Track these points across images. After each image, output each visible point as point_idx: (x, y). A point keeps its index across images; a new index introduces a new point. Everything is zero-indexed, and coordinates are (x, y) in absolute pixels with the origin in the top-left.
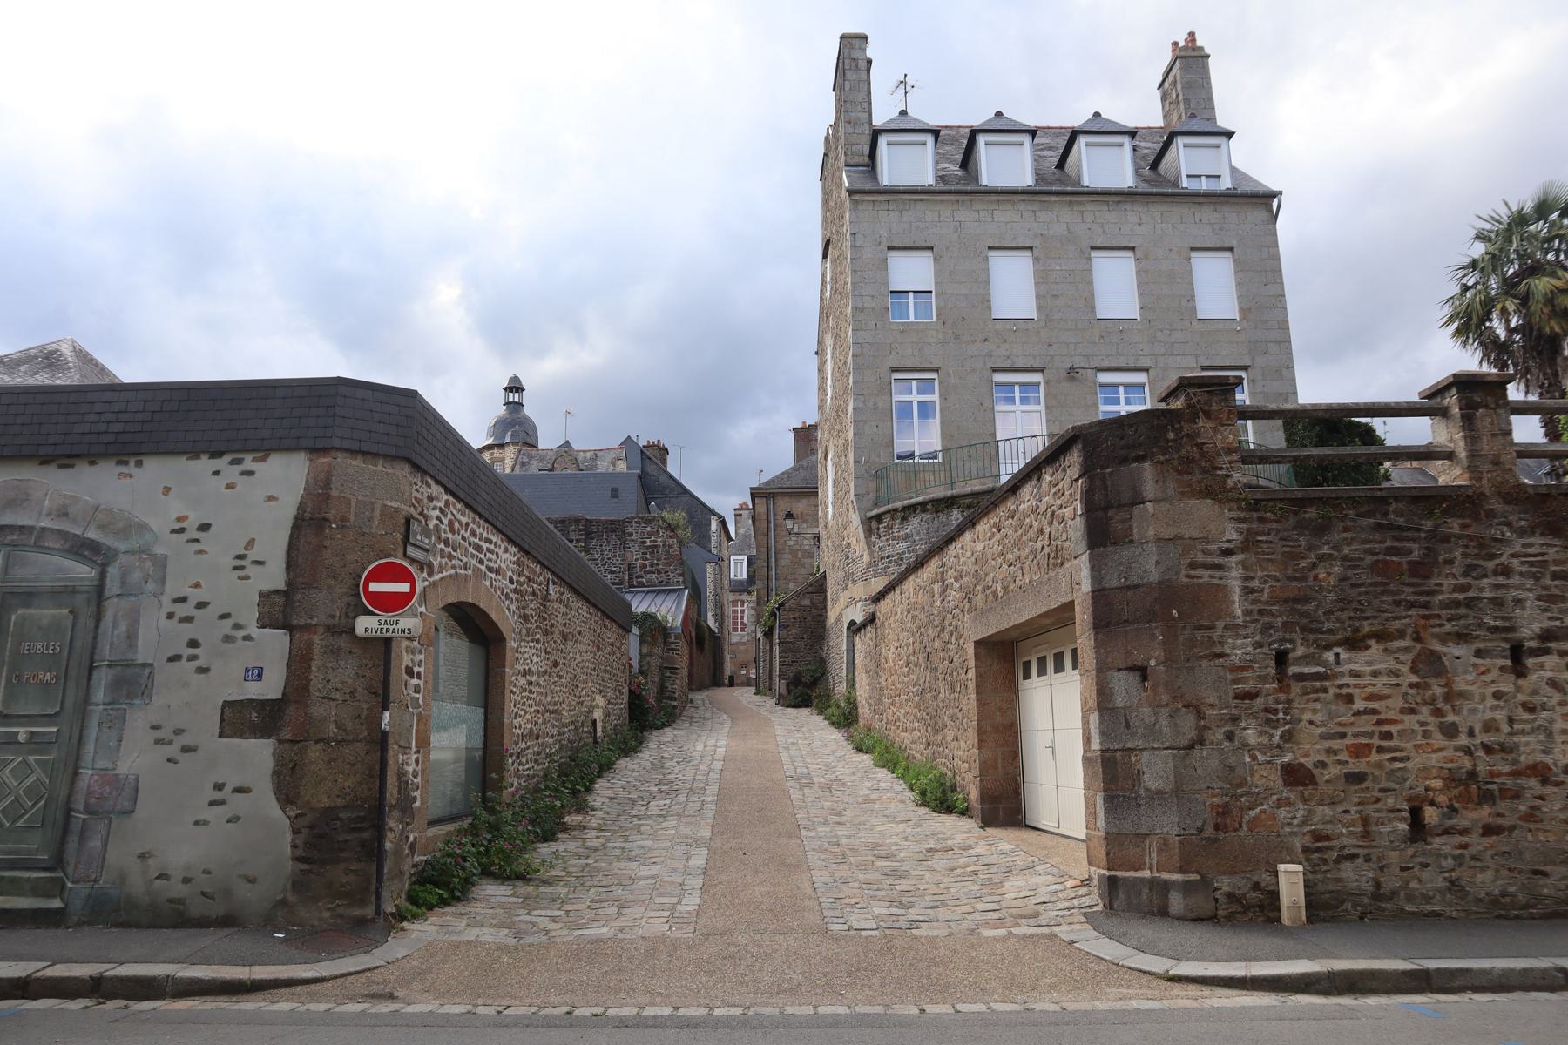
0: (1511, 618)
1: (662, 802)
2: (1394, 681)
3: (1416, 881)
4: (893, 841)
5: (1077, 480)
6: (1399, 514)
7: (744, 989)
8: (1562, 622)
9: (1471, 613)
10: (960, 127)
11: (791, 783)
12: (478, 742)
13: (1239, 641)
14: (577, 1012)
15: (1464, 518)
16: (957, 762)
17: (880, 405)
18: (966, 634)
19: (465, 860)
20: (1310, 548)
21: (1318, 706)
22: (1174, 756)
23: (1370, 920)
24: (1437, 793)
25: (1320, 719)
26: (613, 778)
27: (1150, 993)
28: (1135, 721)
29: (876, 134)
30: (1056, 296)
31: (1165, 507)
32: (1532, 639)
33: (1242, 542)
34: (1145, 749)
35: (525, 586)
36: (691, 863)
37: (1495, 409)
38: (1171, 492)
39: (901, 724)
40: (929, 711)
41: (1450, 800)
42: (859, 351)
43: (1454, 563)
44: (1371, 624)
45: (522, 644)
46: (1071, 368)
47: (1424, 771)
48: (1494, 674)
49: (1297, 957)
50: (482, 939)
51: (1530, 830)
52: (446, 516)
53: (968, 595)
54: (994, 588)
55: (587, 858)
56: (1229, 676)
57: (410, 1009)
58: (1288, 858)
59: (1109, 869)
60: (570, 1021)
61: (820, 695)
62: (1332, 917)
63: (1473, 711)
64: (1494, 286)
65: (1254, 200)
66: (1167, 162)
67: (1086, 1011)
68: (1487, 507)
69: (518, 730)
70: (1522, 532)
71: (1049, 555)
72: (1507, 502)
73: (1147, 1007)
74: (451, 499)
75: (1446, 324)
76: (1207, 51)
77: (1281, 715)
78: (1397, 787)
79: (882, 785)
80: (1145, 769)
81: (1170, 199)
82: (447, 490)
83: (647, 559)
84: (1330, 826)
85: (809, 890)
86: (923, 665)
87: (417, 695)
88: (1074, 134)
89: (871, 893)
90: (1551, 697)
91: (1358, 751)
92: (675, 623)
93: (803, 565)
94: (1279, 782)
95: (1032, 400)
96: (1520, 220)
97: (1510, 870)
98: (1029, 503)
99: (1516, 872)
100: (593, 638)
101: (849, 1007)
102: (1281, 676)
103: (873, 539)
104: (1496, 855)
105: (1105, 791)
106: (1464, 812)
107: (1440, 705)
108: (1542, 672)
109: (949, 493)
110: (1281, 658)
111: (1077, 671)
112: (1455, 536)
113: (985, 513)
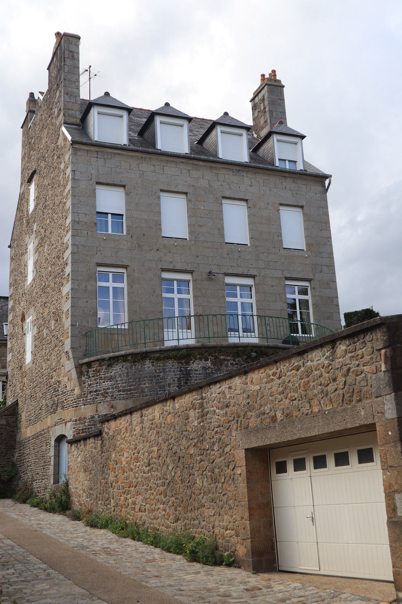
5: (379, 350)
17: (89, 287)
29: (90, 105)
30: (201, 226)
42: (76, 250)
46: (210, 272)
66: (265, 149)
76: (283, 83)
81: (268, 172)
88: (214, 124)
95: (183, 291)
103: (83, 378)
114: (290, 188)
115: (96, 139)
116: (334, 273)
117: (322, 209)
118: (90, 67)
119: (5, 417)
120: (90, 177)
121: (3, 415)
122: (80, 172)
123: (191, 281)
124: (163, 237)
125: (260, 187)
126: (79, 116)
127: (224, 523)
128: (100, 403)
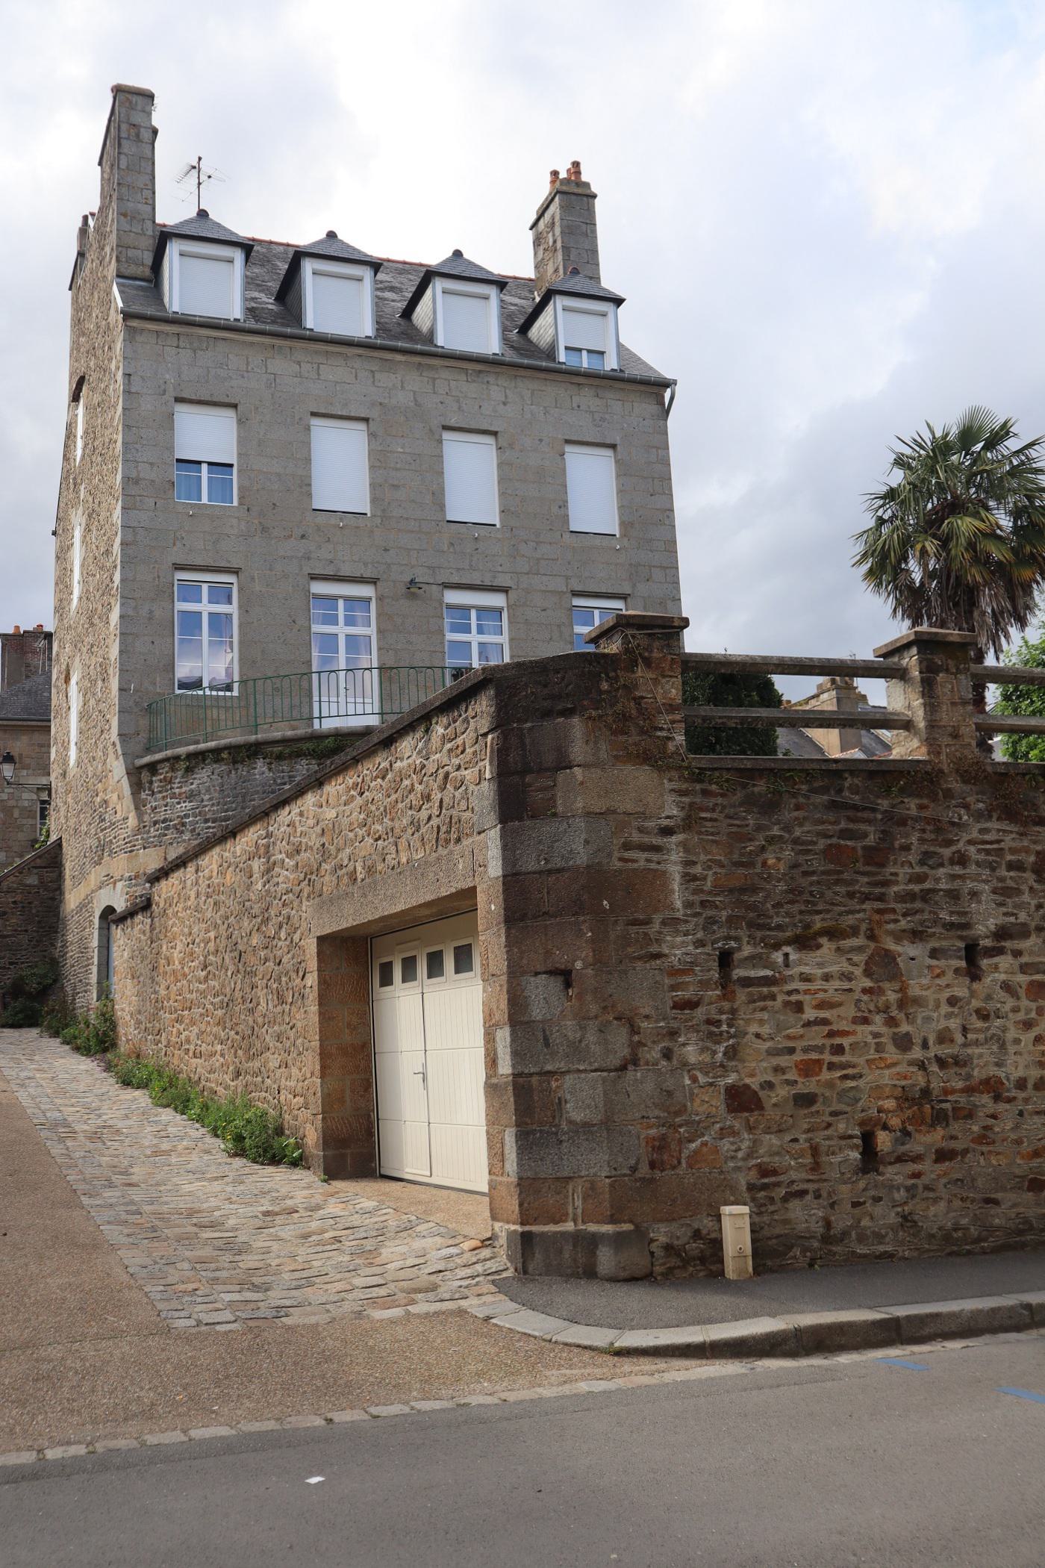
0: (966, 913)
2: (846, 985)
3: (868, 1218)
4: (214, 1204)
5: (485, 735)
6: (855, 790)
7: (76, 1419)
8: (1016, 919)
9: (928, 908)
10: (271, 242)
11: (44, 1134)
13: (679, 939)
15: (921, 797)
17: (157, 613)
18: (304, 925)
20: (759, 828)
21: (765, 1016)
22: (604, 1080)
23: (820, 1266)
24: (890, 1115)
25: (768, 1031)
27: (598, 1371)
28: (555, 1037)
29: (165, 237)
30: (396, 487)
31: (596, 773)
32: (987, 937)
33: (683, 820)
34: (568, 1072)
37: (955, 674)
38: (603, 755)
39: (192, 1047)
41: (903, 1122)
43: (910, 849)
44: (823, 920)
46: (412, 582)
47: (877, 1090)
48: (950, 976)
49: (756, 1315)
51: (983, 1154)
53: (309, 875)
54: (351, 868)
56: (666, 981)
58: (732, 1198)
59: (522, 1224)
61: (53, 1011)
62: (780, 1266)
63: (928, 1019)
64: (912, 522)
65: (642, 388)
66: (540, 328)
68: (945, 786)
70: (979, 816)
71: (438, 827)
72: (965, 782)
73: (600, 1389)
75: (859, 562)
76: (594, 189)
77: (724, 1027)
78: (848, 1109)
80: (568, 1097)
81: (542, 375)
84: (777, 1158)
85: (125, 1278)
86: (231, 968)
88: (429, 276)
89: (211, 1275)
90: (1004, 1003)
91: (808, 1069)
93: (20, 828)
94: (723, 1107)
95: (360, 620)
96: (942, 448)
97: (962, 1199)
98: (410, 761)
99: (968, 1202)
102: (725, 982)
103: (143, 796)
104: (949, 1183)
105: (517, 1126)
106: (917, 1135)
107: (894, 1013)
108: (996, 975)
109: (253, 738)
110: (725, 960)
112: (912, 819)
114: (589, 407)
115: (175, 308)
117: (654, 450)
118: (200, 159)
119: (35, 871)
120: (163, 387)
121: (33, 867)
122: (141, 377)
123: (374, 599)
124: (314, 510)
125: (525, 406)
126: (148, 258)
127: (292, 1083)
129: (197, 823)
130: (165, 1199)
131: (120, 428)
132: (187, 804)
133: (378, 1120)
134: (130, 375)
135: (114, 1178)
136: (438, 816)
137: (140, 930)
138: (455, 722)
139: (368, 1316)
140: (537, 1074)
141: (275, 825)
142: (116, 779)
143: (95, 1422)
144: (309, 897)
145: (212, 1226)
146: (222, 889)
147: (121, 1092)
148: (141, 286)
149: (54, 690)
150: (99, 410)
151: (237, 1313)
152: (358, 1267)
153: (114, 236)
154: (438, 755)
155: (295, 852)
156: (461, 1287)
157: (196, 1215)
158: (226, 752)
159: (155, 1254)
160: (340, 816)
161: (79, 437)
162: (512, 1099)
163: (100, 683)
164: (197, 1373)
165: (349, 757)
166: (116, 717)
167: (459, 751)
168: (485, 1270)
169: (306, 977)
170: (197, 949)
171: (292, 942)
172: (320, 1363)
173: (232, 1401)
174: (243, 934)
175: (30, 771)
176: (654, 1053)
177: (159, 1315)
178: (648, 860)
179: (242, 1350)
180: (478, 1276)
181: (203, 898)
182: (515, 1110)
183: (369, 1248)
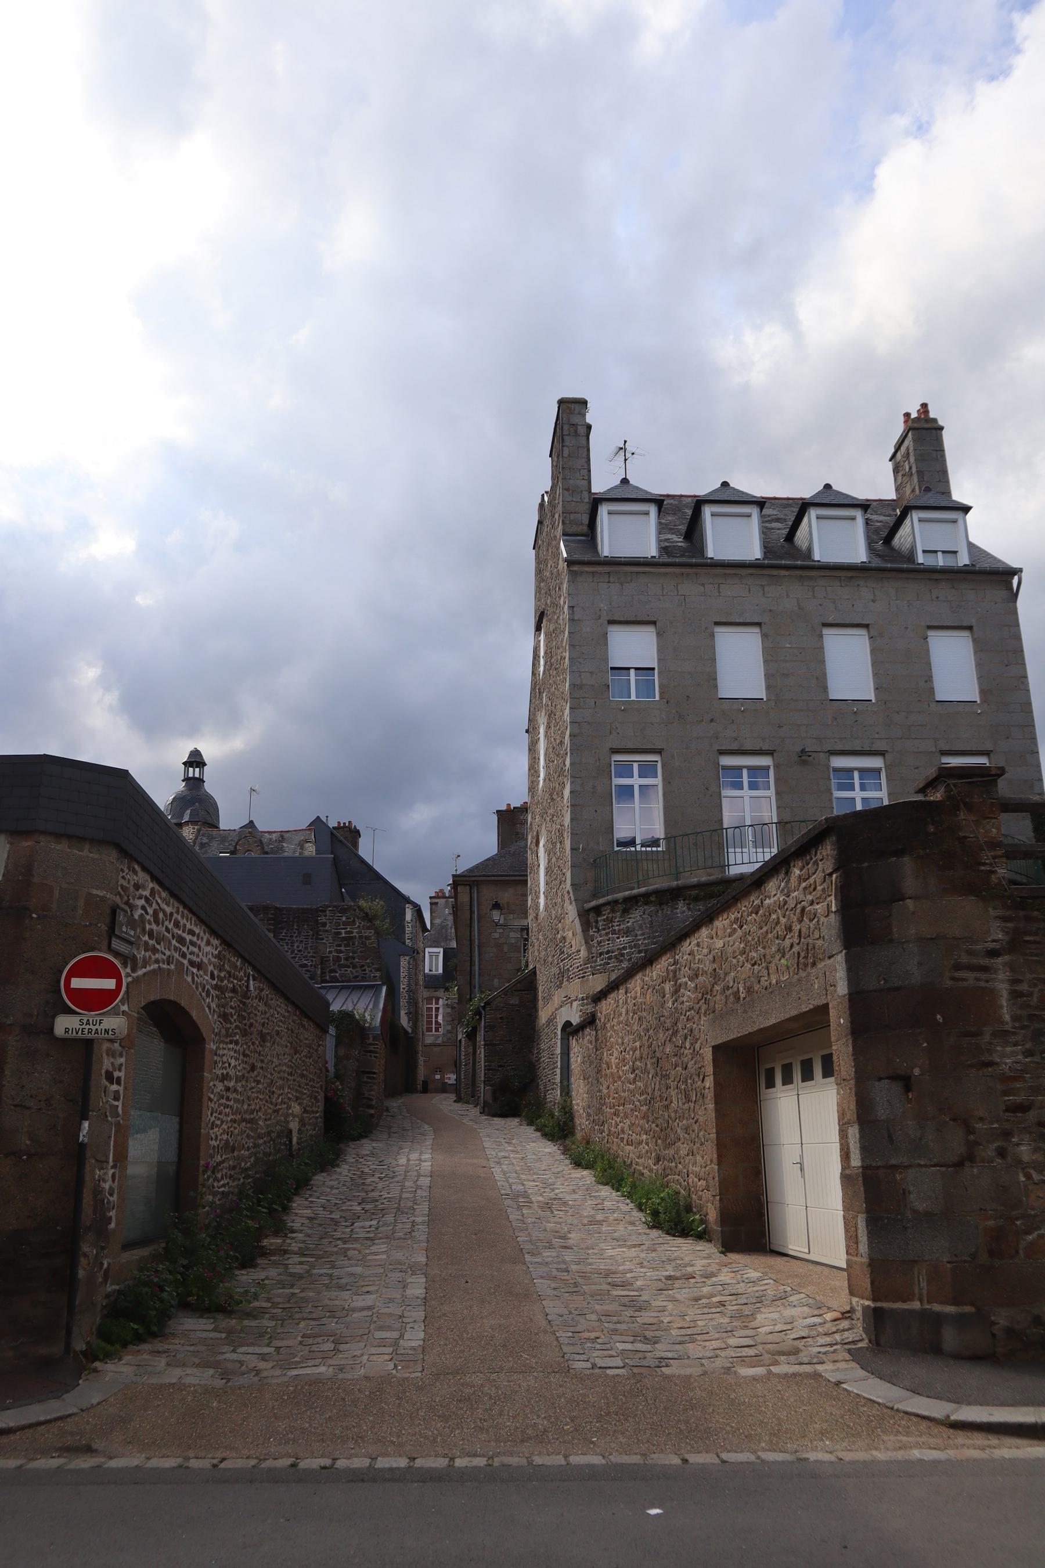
1: (368, 1223)
4: (626, 1267)
5: (830, 875)
7: (483, 1436)
10: (682, 496)
12: (172, 1155)
13: (1009, 1049)
14: (302, 1465)
16: (692, 1179)
19: (162, 1289)
26: (311, 1196)
27: (932, 1441)
29: (596, 502)
30: (785, 675)
34: (910, 1166)
35: (226, 982)
36: (409, 1292)
39: (626, 1136)
40: (659, 1121)
45: (221, 1046)
46: (803, 751)
50: (187, 1380)
52: (151, 905)
53: (705, 994)
55: (292, 1286)
57: (113, 1464)
59: (874, 1300)
60: (294, 1475)
67: (865, 1461)
69: (214, 1142)
71: (799, 953)
73: (931, 1458)
74: (157, 887)
76: (941, 423)
79: (607, 1204)
80: (911, 1189)
81: (904, 575)
82: (154, 878)
83: (341, 952)
85: (543, 1323)
86: (652, 1072)
87: (116, 1103)
88: (804, 506)
89: (612, 1326)
92: (373, 1024)
95: (761, 785)
98: (776, 898)
100: (291, 1039)
101: (604, 1457)
111: (832, 1079)
113: (726, 907)
116: (1035, 738)
118: (625, 442)
124: (720, 699)
126: (585, 518)
128: (613, 971)
129: (633, 954)
130: (590, 1261)
131: (567, 648)
132: (624, 938)
133: (767, 1202)
134: (573, 607)
135: (554, 1241)
136: (798, 944)
137: (588, 1040)
138: (808, 864)
139: (735, 1373)
140: (883, 1167)
141: (680, 954)
142: (571, 920)
143: (498, 1441)
144: (705, 1013)
145: (623, 1285)
146: (644, 1006)
147: (573, 1171)
148: (581, 540)
149: (529, 852)
150: (554, 635)
151: (626, 1361)
152: (735, 1329)
153: (560, 505)
154: (796, 893)
155: (695, 977)
156: (819, 1353)
157: (611, 1276)
158: (654, 896)
159: (571, 1306)
160: (726, 946)
161: (541, 657)
162: (862, 1189)
163: (558, 844)
164: (585, 1409)
165: (730, 897)
166: (570, 871)
167: (812, 889)
168: (843, 1340)
169: (705, 1080)
170: (627, 1056)
171: (694, 1050)
172: (687, 1409)
173: (609, 1435)
174: (660, 1044)
175: (515, 916)
176: (989, 1151)
177: (563, 1357)
178: (977, 979)
179: (624, 1392)
180: (836, 1344)
181: (631, 1014)
182: (865, 1198)
183: (747, 1313)
